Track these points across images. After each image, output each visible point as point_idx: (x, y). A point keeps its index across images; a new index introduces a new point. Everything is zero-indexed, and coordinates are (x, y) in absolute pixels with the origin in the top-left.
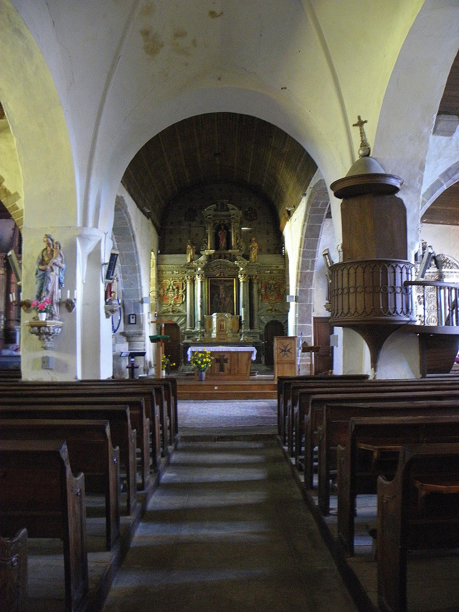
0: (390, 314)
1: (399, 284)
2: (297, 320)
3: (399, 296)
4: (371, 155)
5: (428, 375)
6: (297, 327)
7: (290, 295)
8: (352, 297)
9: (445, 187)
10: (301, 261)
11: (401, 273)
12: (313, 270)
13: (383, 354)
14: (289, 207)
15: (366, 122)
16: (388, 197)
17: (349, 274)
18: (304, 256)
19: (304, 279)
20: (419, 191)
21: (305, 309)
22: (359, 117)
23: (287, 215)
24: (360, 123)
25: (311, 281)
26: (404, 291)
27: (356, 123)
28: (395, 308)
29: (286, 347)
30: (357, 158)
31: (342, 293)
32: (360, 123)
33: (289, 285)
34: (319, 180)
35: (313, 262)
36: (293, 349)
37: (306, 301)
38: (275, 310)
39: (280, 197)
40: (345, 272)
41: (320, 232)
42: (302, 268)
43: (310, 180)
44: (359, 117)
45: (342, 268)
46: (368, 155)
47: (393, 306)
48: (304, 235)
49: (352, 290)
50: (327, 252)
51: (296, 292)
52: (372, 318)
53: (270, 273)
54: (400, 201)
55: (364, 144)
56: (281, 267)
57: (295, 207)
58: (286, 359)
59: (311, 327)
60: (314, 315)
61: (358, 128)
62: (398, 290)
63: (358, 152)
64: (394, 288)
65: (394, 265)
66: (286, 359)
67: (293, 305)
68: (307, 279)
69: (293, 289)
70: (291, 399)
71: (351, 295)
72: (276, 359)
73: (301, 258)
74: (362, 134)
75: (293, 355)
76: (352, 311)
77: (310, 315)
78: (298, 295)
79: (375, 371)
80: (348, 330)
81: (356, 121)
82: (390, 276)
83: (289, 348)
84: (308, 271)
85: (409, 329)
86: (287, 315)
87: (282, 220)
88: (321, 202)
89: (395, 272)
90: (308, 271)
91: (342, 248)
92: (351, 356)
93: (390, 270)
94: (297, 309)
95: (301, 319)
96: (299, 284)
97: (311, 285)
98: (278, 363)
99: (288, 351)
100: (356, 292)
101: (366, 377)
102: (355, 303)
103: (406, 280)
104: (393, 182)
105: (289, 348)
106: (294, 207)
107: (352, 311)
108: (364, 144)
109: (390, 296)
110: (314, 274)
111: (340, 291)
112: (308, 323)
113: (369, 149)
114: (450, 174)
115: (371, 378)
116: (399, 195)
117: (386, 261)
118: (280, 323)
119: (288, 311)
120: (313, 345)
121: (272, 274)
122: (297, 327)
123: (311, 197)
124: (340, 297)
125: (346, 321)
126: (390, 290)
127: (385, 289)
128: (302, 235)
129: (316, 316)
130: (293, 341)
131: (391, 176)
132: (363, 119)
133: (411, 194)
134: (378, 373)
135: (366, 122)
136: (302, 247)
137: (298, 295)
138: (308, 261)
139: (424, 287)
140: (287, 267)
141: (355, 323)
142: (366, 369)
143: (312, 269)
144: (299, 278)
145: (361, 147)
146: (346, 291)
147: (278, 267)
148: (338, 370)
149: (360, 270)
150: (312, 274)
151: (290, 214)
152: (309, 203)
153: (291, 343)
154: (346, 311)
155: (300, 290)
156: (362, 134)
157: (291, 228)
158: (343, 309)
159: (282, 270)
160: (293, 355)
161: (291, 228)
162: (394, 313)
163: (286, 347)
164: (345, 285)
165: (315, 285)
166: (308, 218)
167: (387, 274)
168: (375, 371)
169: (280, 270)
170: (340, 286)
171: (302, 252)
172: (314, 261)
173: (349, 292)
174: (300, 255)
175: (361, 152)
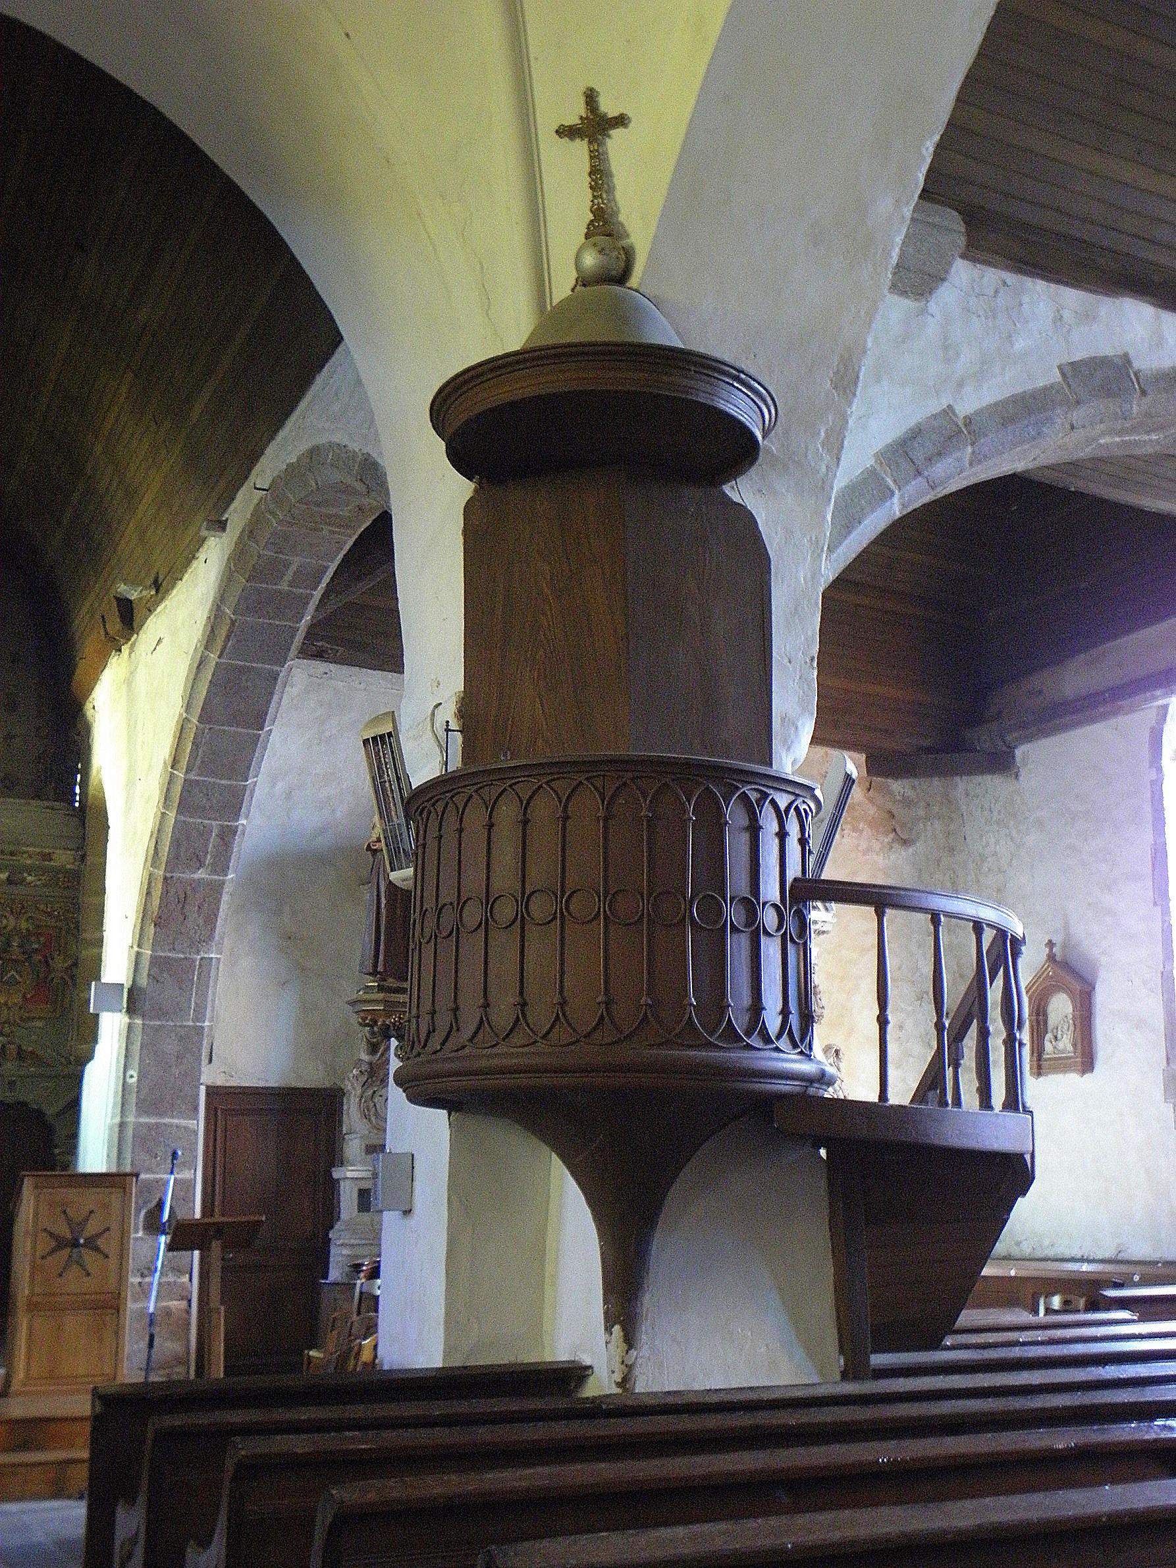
0: (731, 1035)
1: (771, 890)
2: (133, 1099)
3: (771, 950)
4: (634, 281)
5: (878, 1360)
6: (129, 1132)
7: (103, 981)
8: (541, 946)
9: (895, 508)
10: (169, 830)
11: (782, 835)
12: (225, 871)
13: (667, 1250)
14: (134, 583)
15: (621, 121)
16: (691, 493)
17: (525, 822)
18: (185, 806)
19: (177, 910)
20: (823, 487)
21: (170, 1046)
22: (591, 97)
23: (114, 625)
24: (595, 126)
25: (211, 920)
26: (791, 924)
27: (572, 120)
28: (757, 1008)
29: (78, 1226)
30: (562, 285)
31: (486, 925)
32: (595, 126)
33: (100, 942)
34: (304, 446)
35: (228, 836)
36: (115, 1233)
37: (179, 1010)
38: (21, 1055)
39: (90, 545)
40: (508, 811)
41: (273, 704)
42: (174, 861)
43: (255, 456)
44: (591, 97)
45: (490, 793)
46: (622, 278)
47: (746, 1001)
48: (198, 710)
49: (539, 908)
50: (387, 728)
51: (136, 970)
52: (650, 1054)
53: (9, 881)
54: (743, 524)
55: (603, 224)
56: (63, 859)
57: (160, 587)
58: (73, 1282)
59: (196, 1133)
60: (211, 1075)
61: (580, 148)
62: (769, 918)
63: (569, 254)
64: (751, 905)
65: (753, 796)
66: (73, 1282)
67: (112, 1027)
68: (192, 910)
69: (117, 962)
70: (142, 1499)
71: (533, 933)
72: (23, 1285)
73: (172, 814)
74: (599, 176)
75: (113, 1262)
76: (541, 1016)
77: (192, 1076)
78: (143, 981)
79: (630, 1341)
80: (474, 1123)
81: (574, 113)
82: (736, 845)
83: (92, 1228)
84: (201, 874)
85: (809, 1118)
86: (77, 1080)
87: (88, 647)
88: (296, 562)
89: (754, 829)
90: (201, 874)
91: (462, 714)
92: (470, 1260)
93: (734, 814)
94: (136, 1047)
95: (149, 1094)
96: (151, 930)
97: (211, 937)
98: (33, 1307)
99: (91, 1244)
100: (562, 917)
101: (571, 1375)
102: (528, 985)
103: (799, 874)
104: (739, 406)
105: (92, 1228)
106: (157, 585)
107: (541, 1016)
108: (603, 224)
109: (737, 948)
110: (227, 889)
111: (473, 914)
112: (181, 1115)
113: (629, 256)
114: (919, 455)
115: (601, 1384)
116: (743, 491)
117: (716, 767)
118: (40, 1114)
119: (90, 1057)
120: (198, 1215)
121: (20, 890)
122: (129, 1132)
123: (251, 532)
124: (473, 946)
125: (502, 1071)
126: (733, 914)
127: (712, 908)
128: (188, 707)
129: (220, 1081)
130: (115, 1199)
131: (738, 376)
132: (609, 107)
133: (790, 499)
134: (643, 1352)
135: (621, 121)
136: (184, 764)
137: (143, 981)
138: (205, 833)
139: (880, 915)
140: (90, 859)
141: (546, 1080)
142: (572, 1324)
143: (221, 867)
144: (156, 902)
145: (587, 236)
146: (506, 911)
147: (48, 857)
148: (413, 1333)
149: (588, 805)
150: (216, 889)
151: (129, 619)
152: (237, 561)
153: (106, 1206)
154: (502, 1015)
155: (154, 961)
156: (599, 176)
157: (129, 682)
158: (486, 1005)
159: (67, 873)
160: (113, 1262)
161: (129, 682)
162: (749, 1034)
163: (78, 1226)
164: (504, 880)
165: (227, 942)
166: (223, 632)
167: (722, 832)
168: (630, 1341)
169: (58, 871)
170: (474, 880)
171: (178, 788)
172: (234, 831)
173: (522, 920)
174: (167, 797)
175: (590, 260)
